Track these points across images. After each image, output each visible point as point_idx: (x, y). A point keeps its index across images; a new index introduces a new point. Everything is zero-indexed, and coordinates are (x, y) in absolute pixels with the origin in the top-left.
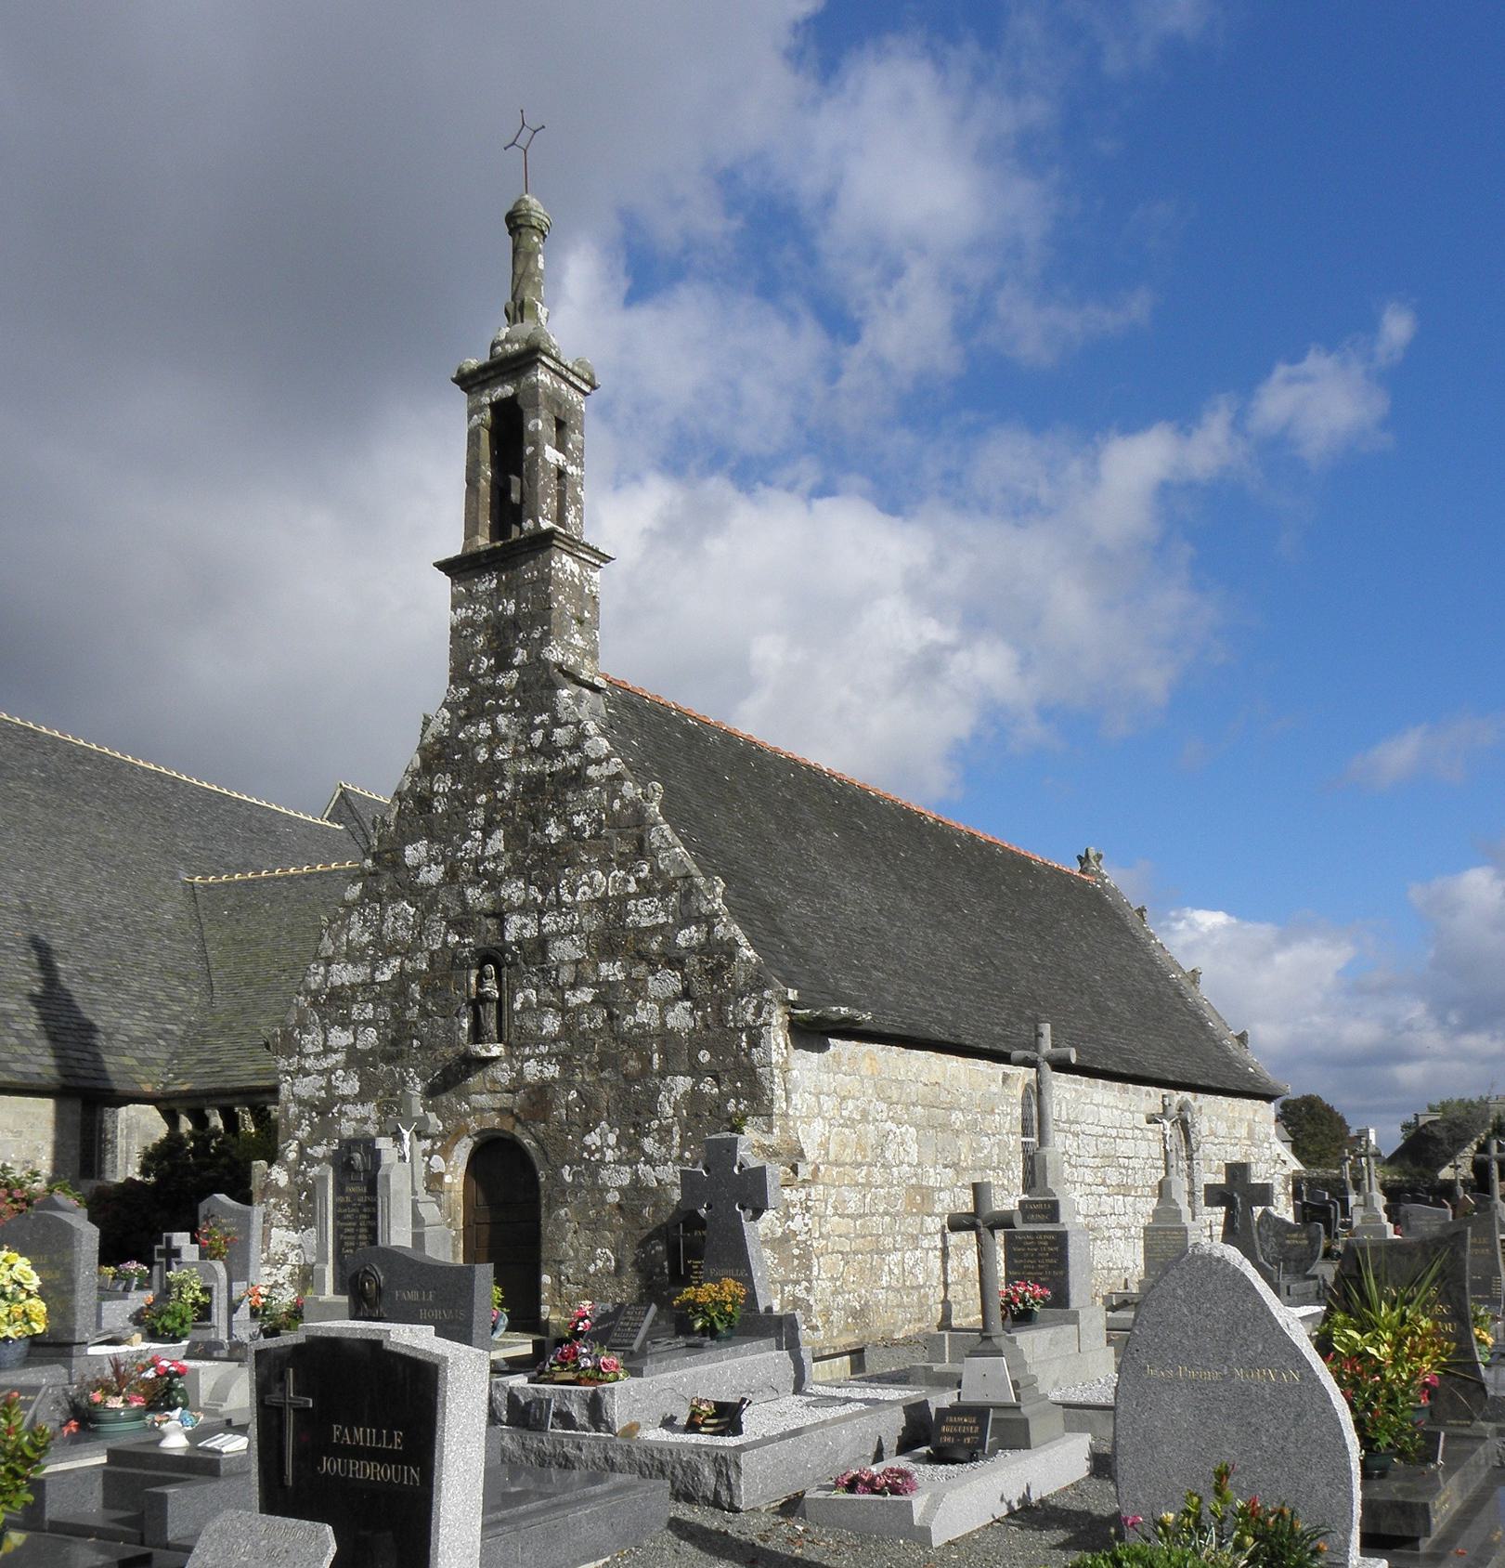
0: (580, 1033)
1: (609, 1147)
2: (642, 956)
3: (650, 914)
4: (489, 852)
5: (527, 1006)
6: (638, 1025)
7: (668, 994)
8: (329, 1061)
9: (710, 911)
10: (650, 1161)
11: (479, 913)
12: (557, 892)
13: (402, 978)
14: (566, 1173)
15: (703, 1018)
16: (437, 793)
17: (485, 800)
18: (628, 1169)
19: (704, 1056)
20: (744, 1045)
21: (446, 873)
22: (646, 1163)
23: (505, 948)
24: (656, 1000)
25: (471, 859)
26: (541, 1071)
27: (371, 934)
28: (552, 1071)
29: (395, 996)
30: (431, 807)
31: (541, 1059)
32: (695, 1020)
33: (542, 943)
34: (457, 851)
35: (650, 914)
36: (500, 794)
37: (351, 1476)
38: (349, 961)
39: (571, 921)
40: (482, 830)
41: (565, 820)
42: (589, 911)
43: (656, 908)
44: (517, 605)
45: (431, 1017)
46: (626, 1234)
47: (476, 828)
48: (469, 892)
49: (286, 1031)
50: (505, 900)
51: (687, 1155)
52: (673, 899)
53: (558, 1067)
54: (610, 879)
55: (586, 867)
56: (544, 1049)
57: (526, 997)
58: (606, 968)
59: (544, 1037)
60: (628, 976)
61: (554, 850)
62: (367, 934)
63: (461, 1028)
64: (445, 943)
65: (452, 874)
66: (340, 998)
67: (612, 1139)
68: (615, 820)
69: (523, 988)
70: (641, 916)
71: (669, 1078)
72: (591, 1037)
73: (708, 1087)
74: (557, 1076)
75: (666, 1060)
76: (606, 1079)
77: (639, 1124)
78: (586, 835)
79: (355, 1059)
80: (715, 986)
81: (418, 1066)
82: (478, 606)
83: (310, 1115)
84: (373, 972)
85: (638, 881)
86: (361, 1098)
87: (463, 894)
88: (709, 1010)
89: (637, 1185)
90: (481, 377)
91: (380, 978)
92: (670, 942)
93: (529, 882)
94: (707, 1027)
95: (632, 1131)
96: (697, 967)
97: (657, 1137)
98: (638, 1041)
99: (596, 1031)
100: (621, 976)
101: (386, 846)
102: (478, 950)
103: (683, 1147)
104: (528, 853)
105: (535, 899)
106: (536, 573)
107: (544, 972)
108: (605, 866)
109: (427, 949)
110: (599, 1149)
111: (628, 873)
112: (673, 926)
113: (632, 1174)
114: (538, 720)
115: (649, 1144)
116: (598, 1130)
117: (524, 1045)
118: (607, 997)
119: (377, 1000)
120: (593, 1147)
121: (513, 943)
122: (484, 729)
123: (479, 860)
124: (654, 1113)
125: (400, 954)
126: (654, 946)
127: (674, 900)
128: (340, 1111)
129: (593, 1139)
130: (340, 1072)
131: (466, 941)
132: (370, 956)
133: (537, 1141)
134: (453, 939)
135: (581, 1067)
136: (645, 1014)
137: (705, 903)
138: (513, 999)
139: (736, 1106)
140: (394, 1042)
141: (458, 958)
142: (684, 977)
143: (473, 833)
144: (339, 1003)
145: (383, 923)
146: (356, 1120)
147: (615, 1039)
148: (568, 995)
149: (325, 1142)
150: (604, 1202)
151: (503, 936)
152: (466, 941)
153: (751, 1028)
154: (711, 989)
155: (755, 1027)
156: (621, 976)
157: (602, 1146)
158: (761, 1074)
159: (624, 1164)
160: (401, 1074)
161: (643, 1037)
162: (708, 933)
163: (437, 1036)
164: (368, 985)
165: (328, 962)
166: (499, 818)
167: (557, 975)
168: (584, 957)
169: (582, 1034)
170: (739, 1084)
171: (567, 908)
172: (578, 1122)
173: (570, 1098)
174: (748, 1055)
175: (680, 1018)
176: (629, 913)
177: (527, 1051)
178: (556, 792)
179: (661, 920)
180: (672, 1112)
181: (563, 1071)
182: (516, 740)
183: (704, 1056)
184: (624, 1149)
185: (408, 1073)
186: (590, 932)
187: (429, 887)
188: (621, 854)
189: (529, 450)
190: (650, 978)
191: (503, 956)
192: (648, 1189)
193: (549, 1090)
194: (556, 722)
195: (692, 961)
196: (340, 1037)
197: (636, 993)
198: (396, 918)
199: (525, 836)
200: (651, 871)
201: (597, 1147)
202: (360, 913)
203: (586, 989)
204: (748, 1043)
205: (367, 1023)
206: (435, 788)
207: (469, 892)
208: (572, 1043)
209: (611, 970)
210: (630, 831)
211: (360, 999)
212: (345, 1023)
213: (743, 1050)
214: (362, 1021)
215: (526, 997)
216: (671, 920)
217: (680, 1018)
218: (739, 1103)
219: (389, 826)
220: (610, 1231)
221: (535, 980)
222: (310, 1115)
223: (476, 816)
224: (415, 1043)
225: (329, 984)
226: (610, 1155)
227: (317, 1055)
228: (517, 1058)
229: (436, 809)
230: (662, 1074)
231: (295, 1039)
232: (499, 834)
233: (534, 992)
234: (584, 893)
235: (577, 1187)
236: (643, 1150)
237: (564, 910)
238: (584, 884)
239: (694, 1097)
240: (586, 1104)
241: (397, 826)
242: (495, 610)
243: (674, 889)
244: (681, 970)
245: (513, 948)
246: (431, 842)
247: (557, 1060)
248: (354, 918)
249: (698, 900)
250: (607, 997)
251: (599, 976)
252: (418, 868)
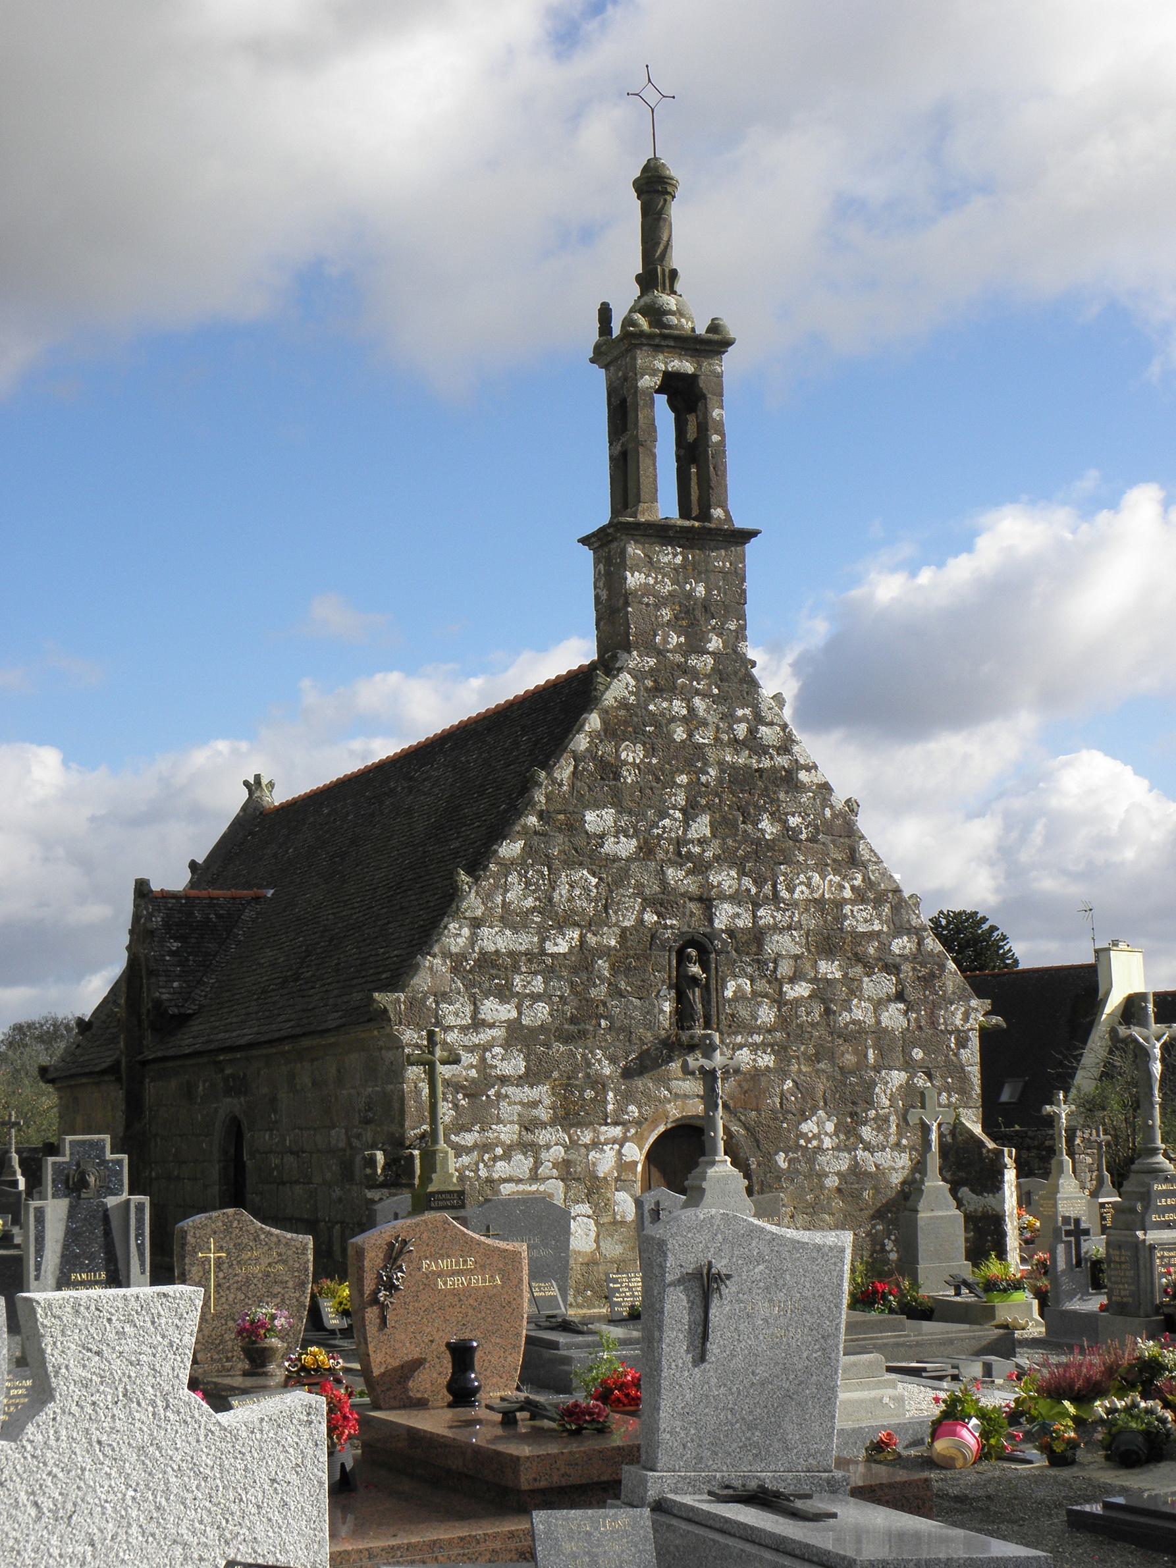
0: (798, 1025)
1: (826, 1134)
2: (859, 959)
3: (866, 921)
4: (693, 834)
5: (739, 996)
6: (854, 1022)
7: (881, 995)
8: (482, 1036)
9: (920, 925)
10: (868, 1147)
11: (682, 895)
12: (774, 886)
13: (584, 957)
14: (781, 1160)
15: (916, 1019)
16: (625, 763)
17: (686, 781)
18: (847, 1156)
19: (917, 1054)
20: (952, 1045)
21: (640, 848)
22: (864, 1149)
23: (712, 936)
24: (869, 999)
25: (671, 839)
26: (754, 1060)
27: (536, 899)
28: (767, 1060)
29: (575, 970)
30: (617, 776)
31: (754, 1048)
32: (909, 1020)
33: (758, 936)
34: (652, 827)
35: (866, 921)
36: (703, 779)
37: (1155, 1218)
38: (506, 926)
39: (790, 917)
40: (683, 811)
41: (778, 817)
42: (807, 910)
43: (871, 916)
44: (708, 590)
45: (625, 997)
46: (845, 1216)
47: (674, 807)
48: (670, 872)
49: (413, 998)
50: (713, 887)
51: (904, 1142)
52: (886, 909)
53: (773, 1057)
54: (826, 882)
55: (803, 868)
56: (758, 1039)
57: (739, 986)
58: (825, 966)
59: (759, 1028)
60: (845, 975)
61: (771, 845)
62: (530, 899)
63: (662, 1011)
64: (640, 921)
65: (647, 850)
66: (494, 965)
67: (830, 1127)
68: (828, 827)
69: (735, 976)
70: (857, 921)
71: (883, 1072)
72: (809, 1030)
73: (921, 1081)
74: (771, 1065)
75: (881, 1054)
76: (823, 1071)
77: (856, 1114)
78: (803, 837)
79: (517, 1035)
80: (927, 993)
81: (607, 1048)
82: (660, 577)
83: (454, 1097)
84: (543, 941)
85: (853, 888)
86: (529, 1078)
87: (663, 873)
88: (923, 1013)
89: (856, 1172)
90: (657, 341)
91: (550, 948)
92: (884, 948)
93: (742, 873)
94: (920, 1028)
95: (849, 1120)
96: (910, 974)
97: (875, 1126)
98: (855, 1035)
99: (813, 1025)
100: (838, 975)
101: (558, 807)
102: (683, 933)
103: (900, 1134)
104: (740, 843)
105: (748, 890)
106: (728, 564)
107: (760, 963)
108: (822, 870)
109: (616, 925)
110: (815, 1137)
111: (843, 879)
112: (888, 934)
113: (851, 1160)
114: (740, 713)
115: (866, 1132)
116: (814, 1118)
117: (736, 1033)
118: (823, 992)
119: (549, 973)
120: (810, 1135)
121: (723, 931)
122: (679, 707)
123: (679, 842)
124: (870, 1103)
125: (579, 926)
126: (871, 951)
127: (886, 910)
128: (498, 1095)
129: (809, 1127)
130: (497, 1050)
131: (669, 922)
132: (536, 923)
133: (747, 1129)
134: (650, 918)
135: (798, 1057)
136: (860, 1012)
137: (915, 917)
138: (724, 987)
139: (948, 1099)
140: (573, 1020)
141: (659, 938)
142: (899, 981)
143: (671, 812)
144: (494, 972)
145: (554, 889)
146: (521, 1103)
147: (831, 1033)
148: (786, 988)
149: (477, 1128)
150: (822, 1187)
151: (711, 921)
152: (669, 922)
153: (959, 1031)
154: (924, 995)
155: (964, 1031)
156: (838, 975)
157: (820, 1134)
158: (969, 1072)
159: (843, 1151)
160: (583, 1055)
161: (859, 1033)
162: (919, 944)
163: (631, 1018)
164: (536, 957)
165: (476, 924)
166: (703, 802)
167: (775, 968)
168: (803, 953)
169: (800, 1026)
170: (950, 1080)
171: (785, 904)
172: (794, 1110)
173: (785, 1087)
174: (956, 1055)
175: (894, 1017)
176: (845, 917)
177: (739, 1039)
178: (766, 789)
179: (877, 927)
180: (888, 1103)
181: (779, 1061)
182: (718, 728)
183: (917, 1054)
184: (842, 1137)
185: (594, 1055)
186: (809, 930)
187: (616, 859)
188: (834, 860)
189: (715, 438)
190: (866, 979)
191: (712, 943)
192: (867, 1174)
193: (762, 1079)
194: (759, 719)
195: (906, 967)
196: (497, 1011)
197: (852, 992)
198: (571, 886)
199: (735, 826)
200: (864, 880)
201: (814, 1135)
202: (520, 874)
203: (804, 984)
204: (956, 1044)
205: (536, 998)
206: (623, 756)
207: (670, 872)
208: (788, 1034)
209: (830, 969)
210: (842, 840)
211: (524, 969)
212: (504, 994)
213: (952, 1050)
214: (528, 995)
215: (739, 986)
216: (885, 929)
217: (894, 1017)
218: (950, 1096)
219: (561, 785)
220: (829, 1214)
221: (749, 970)
222: (454, 1097)
223: (675, 795)
224: (603, 1023)
225: (477, 949)
226: (828, 1143)
227: (464, 1029)
228: (727, 1046)
229: (625, 778)
230: (877, 1069)
231: (429, 1009)
232: (705, 819)
233: (748, 982)
234: (801, 893)
235: (792, 1173)
236: (860, 1136)
237: (782, 905)
238: (802, 883)
239: (908, 1089)
240: (801, 1092)
241: (572, 787)
242: (682, 588)
243: (886, 901)
244: (897, 975)
245: (723, 935)
246: (618, 812)
247: (772, 1050)
248: (513, 878)
249: (908, 913)
250: (823, 992)
251: (817, 972)
252: (602, 836)
